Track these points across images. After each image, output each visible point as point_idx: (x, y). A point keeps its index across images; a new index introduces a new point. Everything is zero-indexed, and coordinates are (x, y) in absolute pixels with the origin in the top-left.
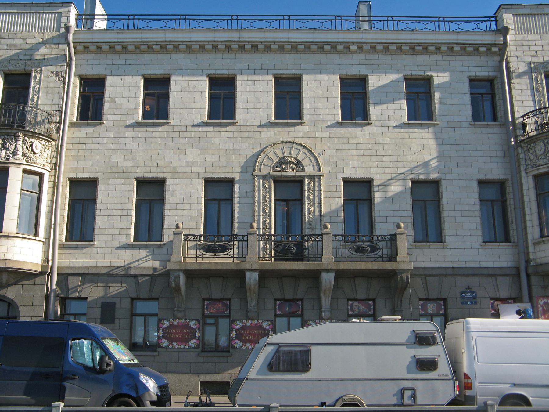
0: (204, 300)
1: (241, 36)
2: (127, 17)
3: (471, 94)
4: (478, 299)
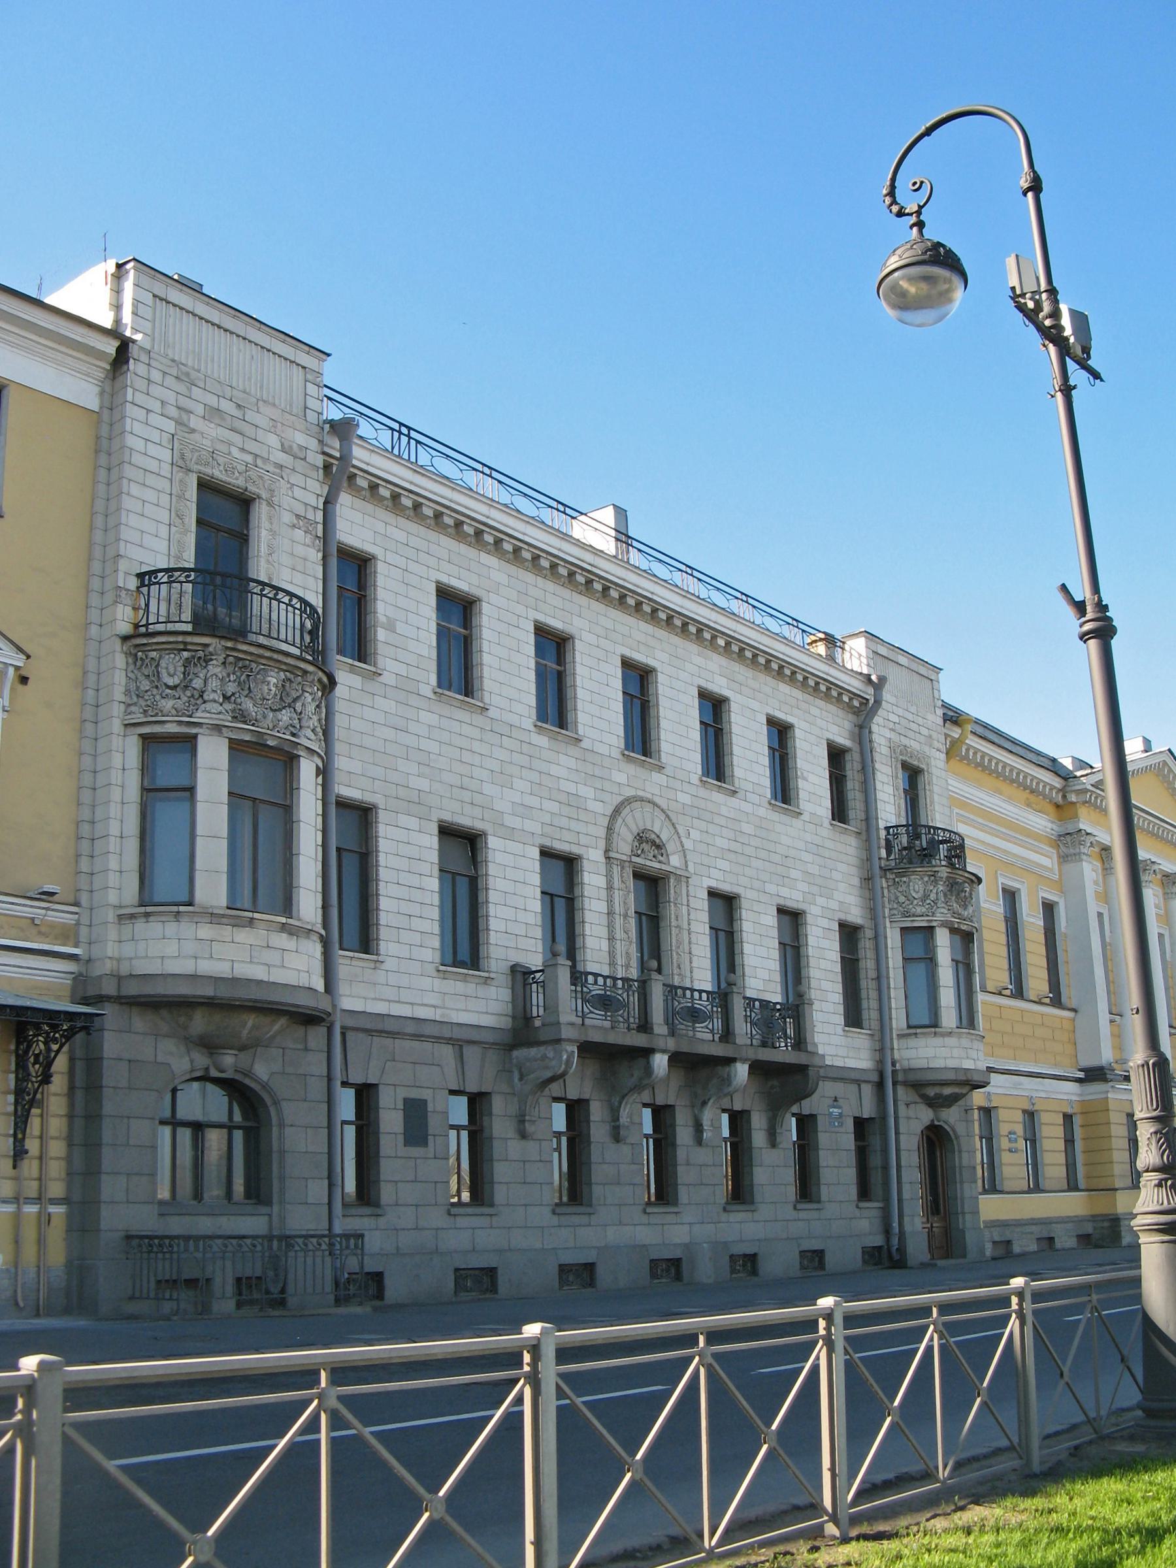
1: (372, 462)
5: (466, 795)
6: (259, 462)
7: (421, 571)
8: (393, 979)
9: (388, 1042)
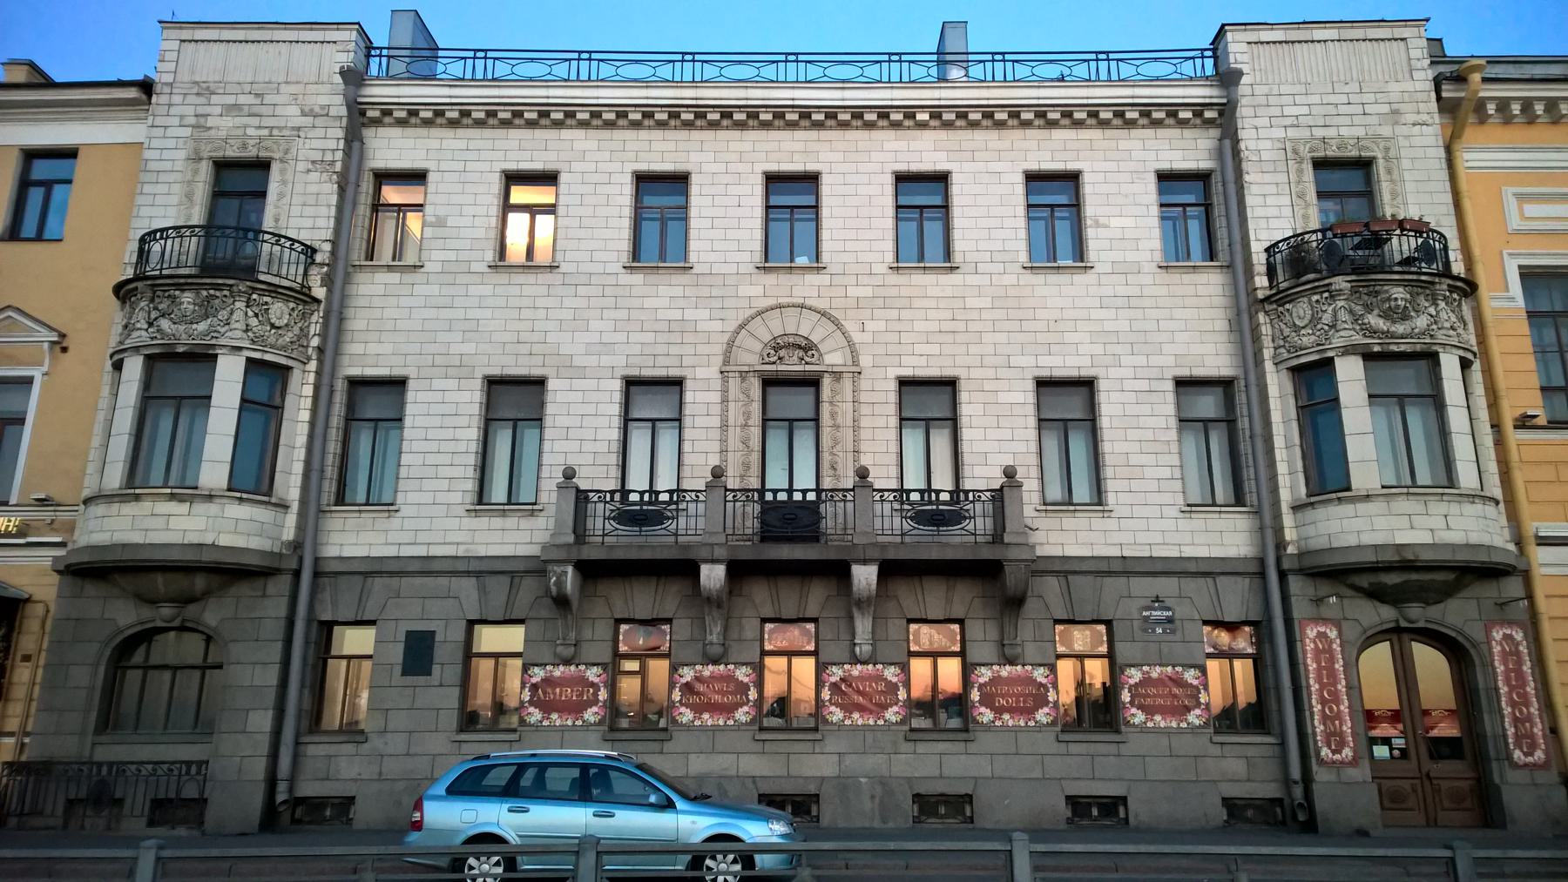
0: (619, 621)
2: (783, 58)
3: (1162, 205)
4: (1178, 623)
5: (524, 349)
6: (275, 132)
7: (485, 166)
8: (408, 524)
9: (395, 581)
